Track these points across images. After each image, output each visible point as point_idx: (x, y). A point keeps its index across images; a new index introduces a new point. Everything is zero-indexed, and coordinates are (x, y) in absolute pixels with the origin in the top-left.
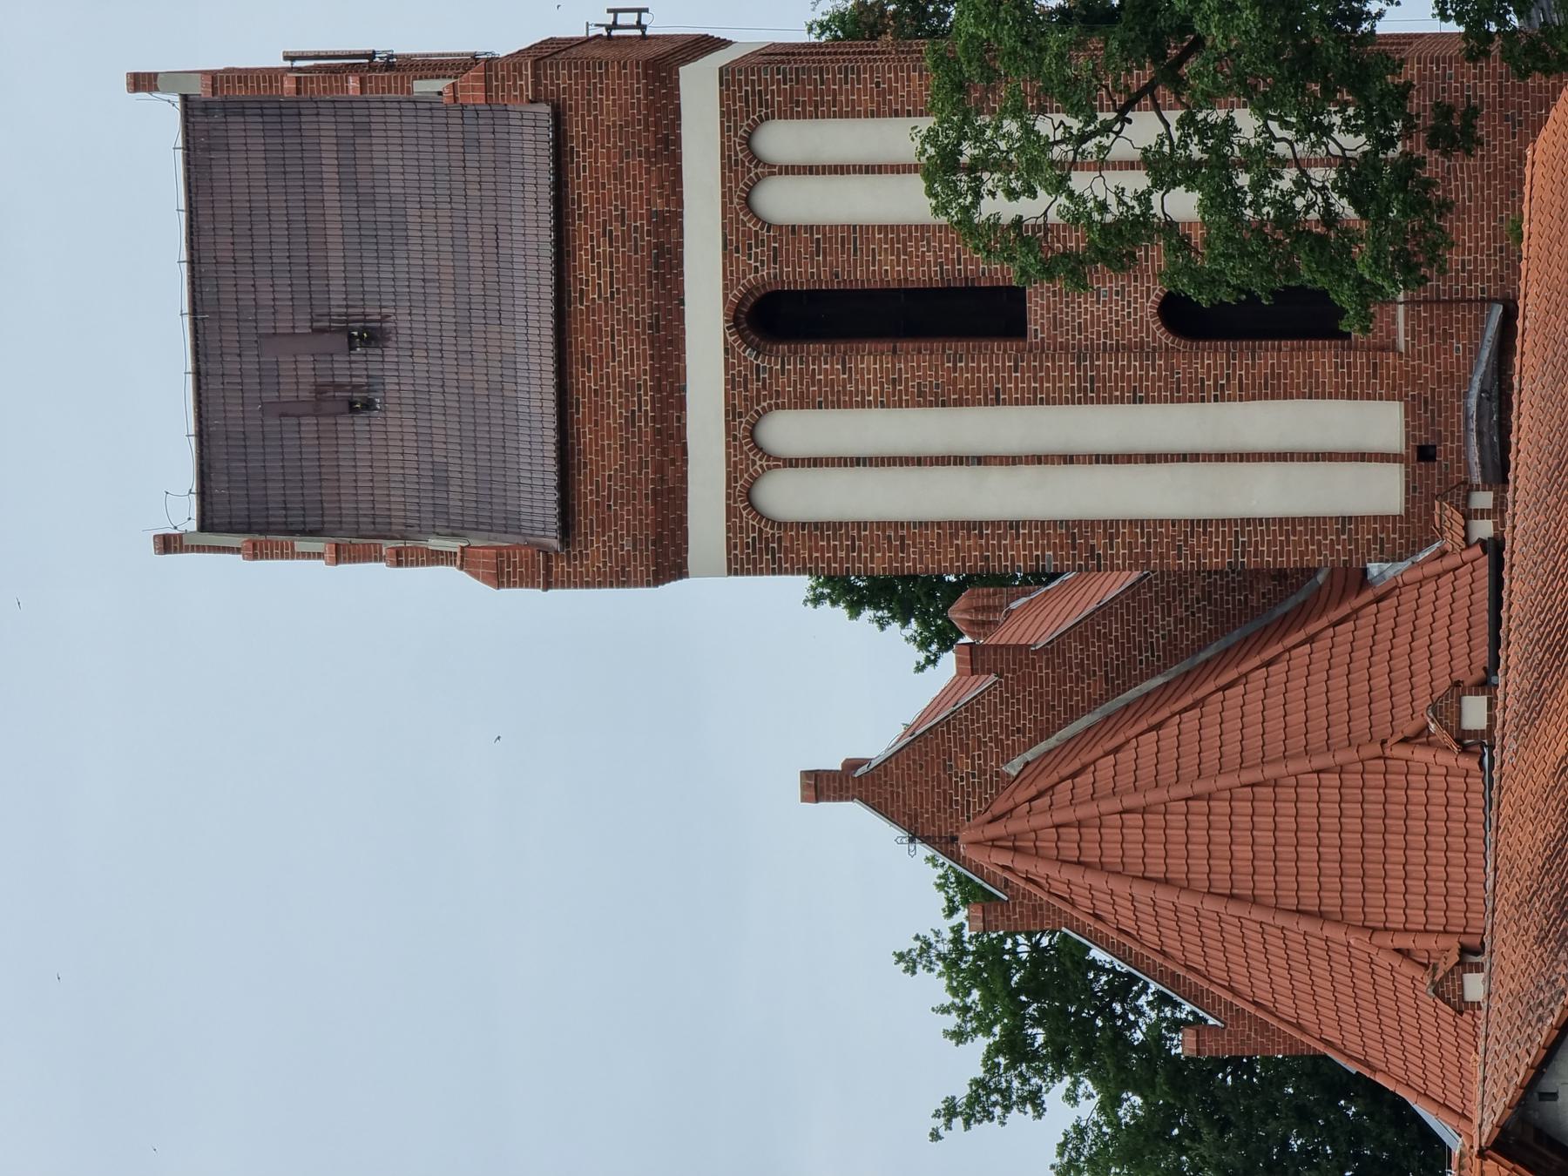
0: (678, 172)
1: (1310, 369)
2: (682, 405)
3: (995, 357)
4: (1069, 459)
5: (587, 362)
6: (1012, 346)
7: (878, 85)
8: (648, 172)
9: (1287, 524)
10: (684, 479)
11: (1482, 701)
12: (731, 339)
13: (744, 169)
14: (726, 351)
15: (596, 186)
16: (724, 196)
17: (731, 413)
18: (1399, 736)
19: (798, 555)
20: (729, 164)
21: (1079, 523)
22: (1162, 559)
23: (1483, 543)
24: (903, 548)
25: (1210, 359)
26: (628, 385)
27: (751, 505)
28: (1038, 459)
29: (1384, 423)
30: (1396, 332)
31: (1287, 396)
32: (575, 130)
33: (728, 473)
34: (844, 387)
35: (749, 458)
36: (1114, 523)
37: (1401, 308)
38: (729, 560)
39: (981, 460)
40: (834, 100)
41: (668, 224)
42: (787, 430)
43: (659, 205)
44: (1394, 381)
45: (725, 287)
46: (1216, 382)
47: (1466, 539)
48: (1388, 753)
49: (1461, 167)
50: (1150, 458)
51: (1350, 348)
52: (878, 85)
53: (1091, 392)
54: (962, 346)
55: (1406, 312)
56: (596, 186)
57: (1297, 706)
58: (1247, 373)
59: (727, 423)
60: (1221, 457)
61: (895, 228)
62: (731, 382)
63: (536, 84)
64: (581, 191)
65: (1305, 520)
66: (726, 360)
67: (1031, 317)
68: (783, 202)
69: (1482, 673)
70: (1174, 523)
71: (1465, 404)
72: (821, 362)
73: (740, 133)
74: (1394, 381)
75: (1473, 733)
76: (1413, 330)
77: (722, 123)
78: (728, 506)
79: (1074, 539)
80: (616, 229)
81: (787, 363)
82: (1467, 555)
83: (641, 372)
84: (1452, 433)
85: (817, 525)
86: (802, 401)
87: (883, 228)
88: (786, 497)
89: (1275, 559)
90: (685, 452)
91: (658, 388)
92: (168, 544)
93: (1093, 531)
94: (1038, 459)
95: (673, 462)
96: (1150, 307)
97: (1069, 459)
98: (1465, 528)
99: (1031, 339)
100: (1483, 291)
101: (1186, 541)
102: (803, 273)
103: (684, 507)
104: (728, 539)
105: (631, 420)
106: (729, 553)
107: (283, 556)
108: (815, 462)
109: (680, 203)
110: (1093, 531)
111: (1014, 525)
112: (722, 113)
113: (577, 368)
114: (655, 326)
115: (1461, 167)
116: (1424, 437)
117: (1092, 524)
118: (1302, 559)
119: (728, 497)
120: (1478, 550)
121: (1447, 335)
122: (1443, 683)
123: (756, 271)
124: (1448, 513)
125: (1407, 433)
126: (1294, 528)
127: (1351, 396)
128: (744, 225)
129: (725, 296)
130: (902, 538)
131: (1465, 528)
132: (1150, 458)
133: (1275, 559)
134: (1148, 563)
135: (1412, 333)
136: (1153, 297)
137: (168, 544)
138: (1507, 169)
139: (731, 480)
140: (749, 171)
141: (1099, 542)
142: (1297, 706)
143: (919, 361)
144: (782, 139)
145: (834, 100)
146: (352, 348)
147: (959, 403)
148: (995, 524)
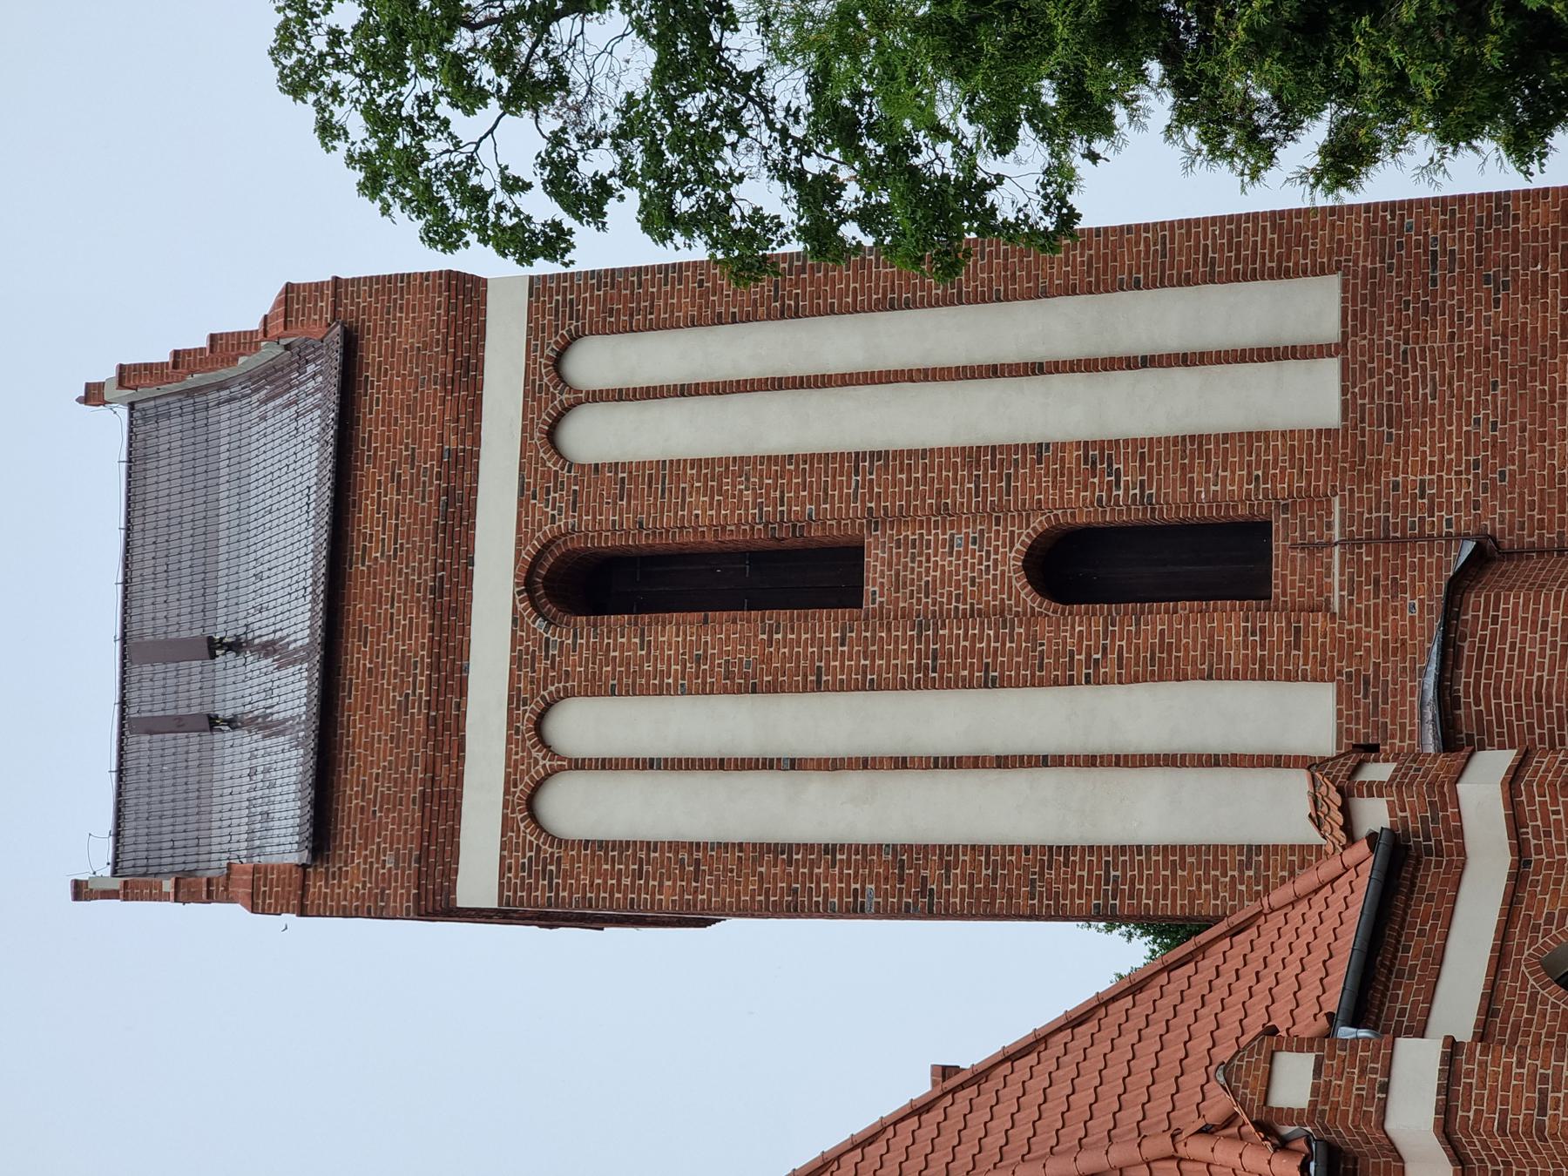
0: (477, 403)
1: (1211, 637)
2: (463, 690)
3: (816, 631)
4: (901, 763)
5: (363, 635)
6: (844, 614)
7: (701, 283)
8: (443, 403)
9: (1174, 854)
10: (459, 781)
11: (1308, 1060)
12: (520, 607)
13: (552, 400)
14: (514, 621)
15: (390, 421)
16: (524, 430)
17: (515, 700)
18: (1200, 1124)
19: (578, 880)
20: (531, 391)
21: (908, 848)
22: (1010, 898)
23: (1372, 838)
24: (697, 875)
25: (1081, 626)
26: (404, 662)
27: (533, 816)
28: (865, 763)
29: (1308, 716)
30: (1330, 588)
31: (1181, 677)
32: (371, 355)
33: (508, 775)
34: (641, 667)
35: (535, 762)
36: (952, 849)
37: (1337, 549)
38: (501, 885)
39: (795, 764)
40: (652, 306)
41: (460, 468)
42: (581, 724)
43: (453, 442)
44: (1324, 652)
45: (519, 542)
46: (1089, 656)
47: (1348, 828)
48: (1182, 1151)
49: (1423, 350)
50: (1003, 762)
51: (1267, 609)
52: (701, 283)
53: (932, 674)
54: (785, 614)
55: (1342, 555)
56: (390, 421)
57: (1090, 1079)
58: (1129, 643)
59: (510, 711)
60: (1091, 761)
61: (709, 462)
62: (517, 661)
63: (335, 305)
64: (371, 425)
65: (1196, 850)
66: (514, 633)
67: (869, 575)
68: (594, 437)
69: (1323, 1022)
70: (1027, 849)
71: (1422, 684)
72: (620, 635)
73: (547, 352)
74: (1324, 652)
75: (1288, 1115)
76: (1351, 580)
77: (528, 341)
78: (505, 817)
79: (902, 868)
80: (406, 472)
81: (582, 638)
82: (1351, 856)
83: (418, 646)
84: (1403, 726)
85: (603, 845)
86: (596, 687)
87: (696, 463)
88: (576, 809)
89: (1156, 901)
90: (462, 747)
91: (436, 666)
92: (81, 891)
93: (926, 858)
94: (865, 763)
95: (448, 759)
96: (1013, 559)
97: (901, 763)
98: (1345, 810)
99: (867, 605)
100: (1449, 524)
101: (1042, 874)
102: (609, 526)
103: (456, 816)
104: (502, 858)
105: (404, 708)
106: (502, 876)
107: (151, 898)
108: (605, 764)
109: (477, 440)
110: (926, 858)
111: (830, 849)
112: (529, 328)
113: (352, 643)
114: (437, 590)
115: (1423, 350)
116: (1362, 732)
117: (925, 849)
118: (1192, 903)
119: (505, 805)
120: (1362, 848)
121: (1399, 589)
122: (1255, 1026)
123: (553, 522)
124: (1324, 789)
125: (1339, 727)
126: (1183, 859)
127: (1264, 675)
128: (544, 465)
129: (518, 553)
130: (697, 862)
131: (1345, 810)
132: (1003, 762)
133: (1156, 901)
134: (993, 903)
135: (1351, 586)
136: (1017, 546)
137: (81, 891)
138: (1487, 350)
139: (510, 784)
140: (554, 397)
141: (932, 872)
142: (1090, 1079)
143: (731, 634)
144: (596, 361)
145: (652, 306)
146: (213, 656)
147: (774, 688)
148: (808, 848)
